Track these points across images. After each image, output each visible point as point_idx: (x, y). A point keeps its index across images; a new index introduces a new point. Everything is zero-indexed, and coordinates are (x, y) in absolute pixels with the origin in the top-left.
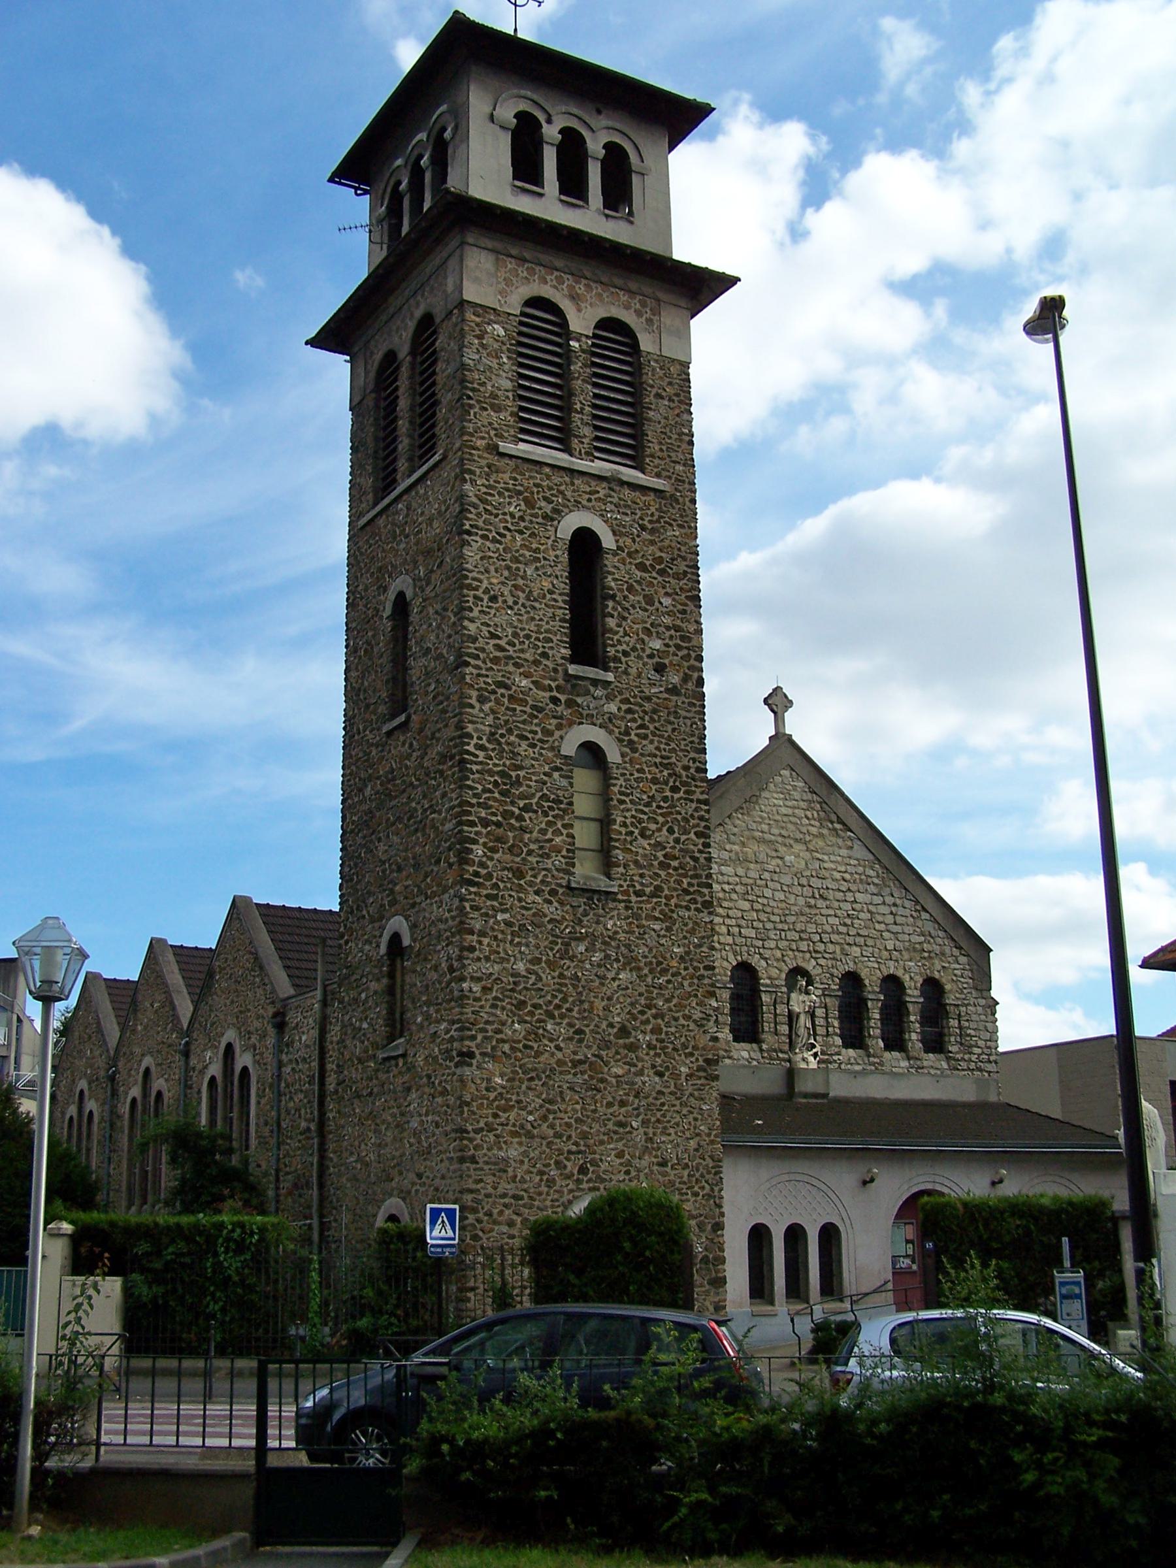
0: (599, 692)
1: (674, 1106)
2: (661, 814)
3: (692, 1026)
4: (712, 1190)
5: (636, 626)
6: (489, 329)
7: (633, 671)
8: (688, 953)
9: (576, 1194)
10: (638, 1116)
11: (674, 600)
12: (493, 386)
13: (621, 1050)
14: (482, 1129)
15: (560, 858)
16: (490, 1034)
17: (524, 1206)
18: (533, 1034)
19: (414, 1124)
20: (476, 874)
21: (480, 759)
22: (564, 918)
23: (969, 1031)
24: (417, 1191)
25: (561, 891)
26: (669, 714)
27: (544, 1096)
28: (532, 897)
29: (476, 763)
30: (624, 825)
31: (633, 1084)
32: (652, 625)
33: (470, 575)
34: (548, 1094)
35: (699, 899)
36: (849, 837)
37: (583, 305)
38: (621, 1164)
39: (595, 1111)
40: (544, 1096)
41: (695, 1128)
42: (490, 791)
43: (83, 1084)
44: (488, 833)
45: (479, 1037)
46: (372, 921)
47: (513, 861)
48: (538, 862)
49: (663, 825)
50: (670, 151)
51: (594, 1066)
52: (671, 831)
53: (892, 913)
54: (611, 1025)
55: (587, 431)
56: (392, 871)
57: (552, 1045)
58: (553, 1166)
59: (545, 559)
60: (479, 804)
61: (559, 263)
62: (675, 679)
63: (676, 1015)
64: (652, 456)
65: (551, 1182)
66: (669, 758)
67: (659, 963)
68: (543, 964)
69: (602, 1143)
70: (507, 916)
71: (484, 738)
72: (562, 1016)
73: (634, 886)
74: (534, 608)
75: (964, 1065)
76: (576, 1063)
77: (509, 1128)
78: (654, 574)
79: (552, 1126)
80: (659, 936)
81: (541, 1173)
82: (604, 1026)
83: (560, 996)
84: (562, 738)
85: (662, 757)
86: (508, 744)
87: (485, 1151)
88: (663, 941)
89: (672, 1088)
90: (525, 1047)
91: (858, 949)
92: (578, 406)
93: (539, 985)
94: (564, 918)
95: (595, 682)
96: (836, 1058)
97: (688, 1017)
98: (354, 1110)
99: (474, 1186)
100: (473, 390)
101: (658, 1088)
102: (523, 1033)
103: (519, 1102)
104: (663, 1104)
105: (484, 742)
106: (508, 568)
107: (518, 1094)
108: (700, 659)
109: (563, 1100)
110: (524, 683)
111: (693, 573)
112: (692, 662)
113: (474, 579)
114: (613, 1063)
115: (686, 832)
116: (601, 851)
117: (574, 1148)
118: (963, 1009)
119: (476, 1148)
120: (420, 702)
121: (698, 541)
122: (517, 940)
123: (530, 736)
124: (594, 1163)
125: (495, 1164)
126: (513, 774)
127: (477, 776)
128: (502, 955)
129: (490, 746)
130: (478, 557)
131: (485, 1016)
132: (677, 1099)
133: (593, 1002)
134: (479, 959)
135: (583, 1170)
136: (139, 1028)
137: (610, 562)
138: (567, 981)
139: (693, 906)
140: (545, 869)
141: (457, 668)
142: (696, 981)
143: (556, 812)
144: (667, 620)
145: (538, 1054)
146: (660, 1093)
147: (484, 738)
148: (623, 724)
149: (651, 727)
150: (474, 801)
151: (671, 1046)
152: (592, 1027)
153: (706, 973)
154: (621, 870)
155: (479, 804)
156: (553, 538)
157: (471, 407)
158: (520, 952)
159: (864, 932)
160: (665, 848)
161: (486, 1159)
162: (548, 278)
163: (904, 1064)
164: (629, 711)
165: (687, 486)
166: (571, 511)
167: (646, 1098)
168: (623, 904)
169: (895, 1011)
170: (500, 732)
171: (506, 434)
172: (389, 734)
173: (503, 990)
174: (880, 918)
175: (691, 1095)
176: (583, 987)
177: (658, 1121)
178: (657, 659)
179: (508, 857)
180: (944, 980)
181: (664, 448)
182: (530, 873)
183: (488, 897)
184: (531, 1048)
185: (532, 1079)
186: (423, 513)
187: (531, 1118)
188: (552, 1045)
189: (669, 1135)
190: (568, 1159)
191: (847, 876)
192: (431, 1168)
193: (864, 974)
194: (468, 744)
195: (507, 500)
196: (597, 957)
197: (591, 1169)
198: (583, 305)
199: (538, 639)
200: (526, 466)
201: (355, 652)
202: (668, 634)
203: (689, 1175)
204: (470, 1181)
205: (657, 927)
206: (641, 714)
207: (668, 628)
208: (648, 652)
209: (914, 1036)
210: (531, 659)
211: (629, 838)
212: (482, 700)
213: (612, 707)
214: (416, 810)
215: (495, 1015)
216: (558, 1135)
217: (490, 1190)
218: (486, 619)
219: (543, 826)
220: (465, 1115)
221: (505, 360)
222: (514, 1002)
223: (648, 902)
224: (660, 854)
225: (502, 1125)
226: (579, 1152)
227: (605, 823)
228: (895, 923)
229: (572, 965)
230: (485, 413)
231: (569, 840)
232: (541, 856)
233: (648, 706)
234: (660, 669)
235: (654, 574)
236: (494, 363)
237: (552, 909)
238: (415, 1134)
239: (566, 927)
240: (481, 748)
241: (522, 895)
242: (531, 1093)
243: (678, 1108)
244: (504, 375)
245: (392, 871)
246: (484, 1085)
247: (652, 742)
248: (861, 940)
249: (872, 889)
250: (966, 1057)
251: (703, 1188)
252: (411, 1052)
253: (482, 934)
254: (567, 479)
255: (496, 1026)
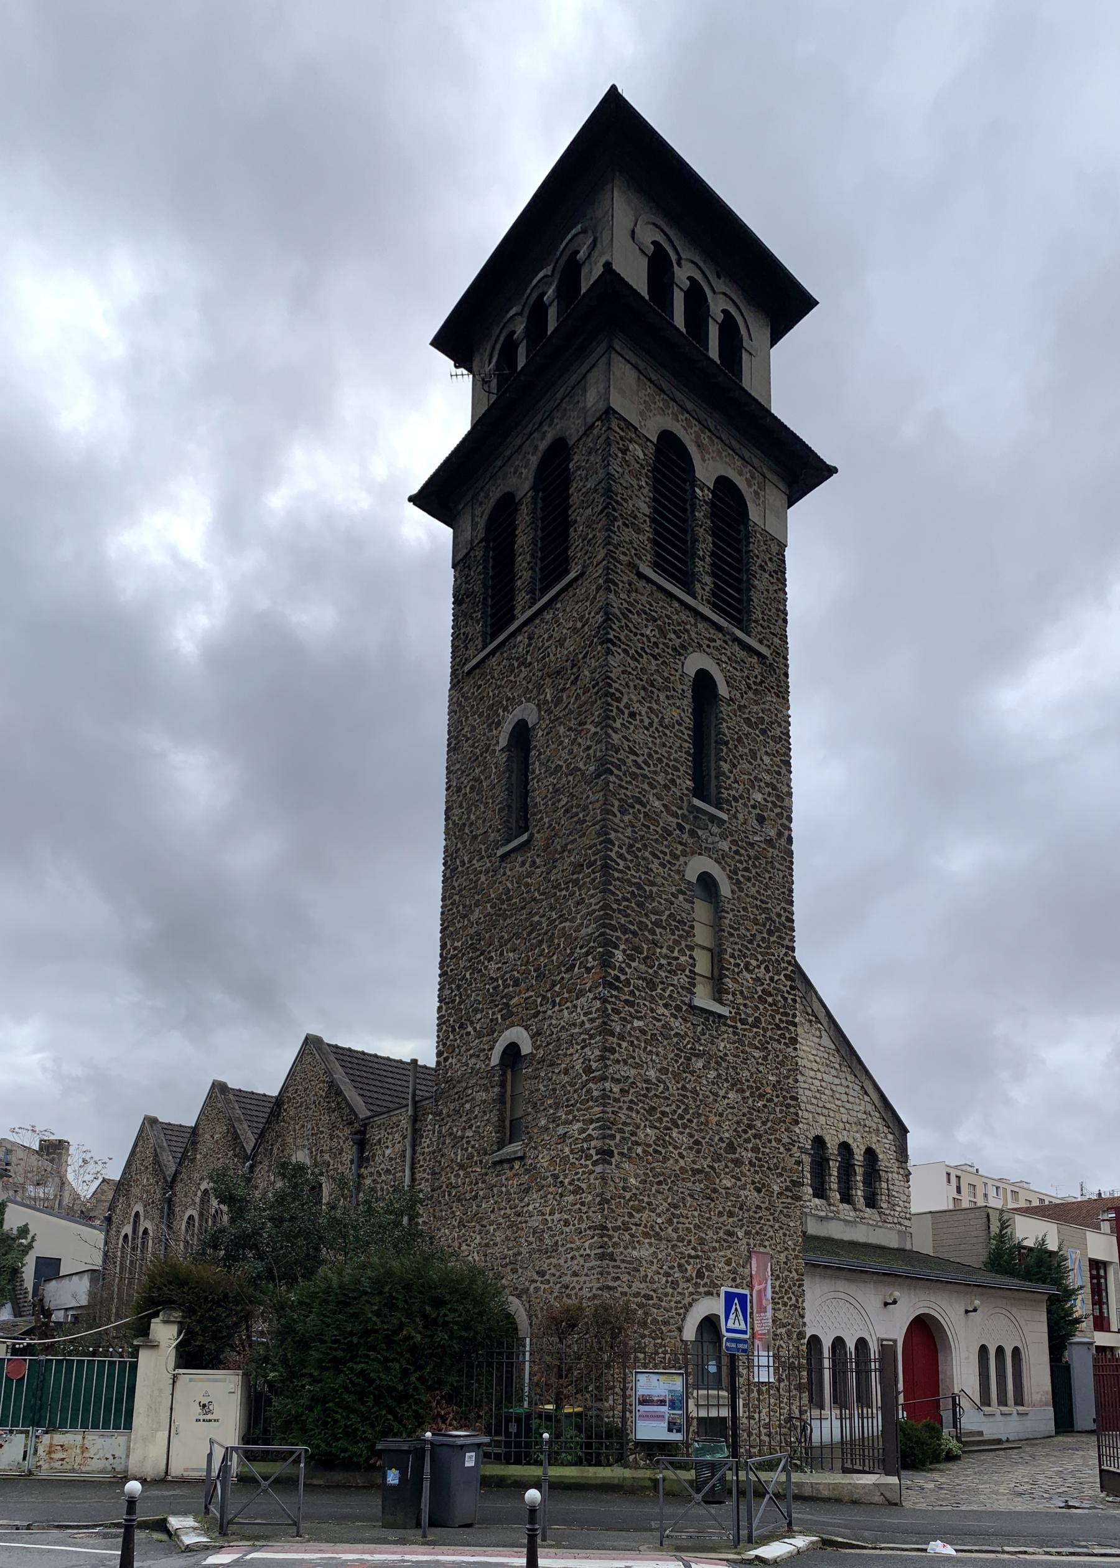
0: (715, 829)
1: (769, 1220)
2: (761, 953)
3: (782, 1149)
4: (797, 1301)
5: (743, 776)
6: (631, 447)
7: (740, 816)
8: (779, 1082)
9: (695, 1297)
10: (742, 1226)
11: (771, 760)
12: (634, 506)
13: (729, 1164)
14: (619, 1228)
15: (683, 976)
16: (627, 1135)
17: (654, 1306)
18: (661, 1141)
19: (535, 1222)
20: (617, 978)
21: (621, 867)
22: (686, 1034)
23: (894, 1193)
24: (537, 1289)
25: (685, 1008)
26: (767, 863)
27: (669, 1200)
28: (661, 1010)
29: (616, 870)
30: (733, 956)
31: (739, 1196)
32: (755, 777)
33: (614, 684)
34: (673, 1199)
35: (787, 1035)
36: (819, 1028)
37: (707, 456)
38: (729, 1271)
39: (709, 1219)
40: (669, 1200)
41: (784, 1242)
42: (627, 900)
43: (139, 1207)
44: (627, 940)
45: (618, 1137)
46: (479, 1035)
47: (647, 972)
48: (667, 977)
49: (762, 962)
50: (772, 346)
51: (707, 1175)
52: (767, 969)
53: (846, 1093)
54: (721, 1140)
55: (708, 579)
56: (506, 986)
57: (676, 1152)
58: (676, 1269)
59: (674, 690)
60: (620, 911)
61: (690, 406)
62: (773, 833)
63: (770, 1137)
64: (756, 622)
65: (675, 1284)
66: (767, 903)
67: (758, 1089)
68: (670, 1075)
69: (715, 1249)
70: (641, 1023)
71: (624, 848)
72: (685, 1126)
73: (740, 1015)
74: (665, 735)
75: (890, 1219)
76: (695, 1172)
77: (641, 1228)
78: (757, 732)
79: (676, 1230)
80: (758, 1063)
81: (667, 1275)
82: (716, 1139)
83: (683, 1107)
84: (686, 863)
85: (761, 901)
86: (644, 859)
87: (621, 1249)
88: (761, 1068)
89: (767, 1205)
90: (656, 1151)
91: (824, 1118)
92: (701, 553)
93: (666, 1094)
94: (686, 1034)
95: (713, 818)
96: (808, 1204)
97: (779, 1141)
98: (453, 1212)
99: (611, 1284)
100: (617, 502)
101: (757, 1203)
102: (654, 1138)
103: (649, 1204)
104: (761, 1218)
105: (624, 851)
106: (644, 689)
107: (649, 1196)
108: (790, 819)
109: (685, 1206)
110: (657, 803)
111: (785, 740)
112: (784, 821)
113: (617, 690)
114: (723, 1176)
115: (778, 974)
116: (712, 978)
117: (693, 1253)
118: (890, 1175)
119: (615, 1245)
120: (546, 820)
121: (790, 712)
122: (649, 1048)
123: (661, 856)
124: (709, 1268)
125: (630, 1263)
126: (648, 888)
127: (618, 883)
128: (637, 1060)
129: (629, 857)
130: (620, 669)
131: (623, 1117)
132: (771, 1214)
133: (708, 1117)
134: (618, 1061)
135: (700, 1275)
136: (198, 1157)
137: (724, 708)
138: (688, 1094)
139: (783, 1041)
140: (673, 985)
141: (598, 776)
142: (784, 1108)
143: (681, 932)
144: (767, 778)
145: (665, 1160)
146: (758, 1207)
147: (624, 848)
148: (733, 863)
149: (754, 872)
150: (615, 906)
151: (766, 1165)
152: (707, 1140)
153: (792, 1103)
154: (730, 997)
155: (620, 911)
156: (680, 672)
157: (616, 519)
158: (651, 1060)
159: (828, 1105)
160: (763, 984)
161: (622, 1257)
162: (680, 417)
163: (852, 1213)
164: (737, 852)
165: (781, 659)
166: (694, 651)
167: (748, 1211)
168: (731, 1029)
169: (847, 1170)
170: (637, 845)
171: (644, 558)
172: (504, 857)
173: (638, 1094)
174: (838, 1096)
175: (781, 1211)
176: (701, 1101)
177: (757, 1233)
178: (758, 811)
179: (643, 967)
180: (878, 1151)
181: (765, 618)
182: (661, 986)
183: (626, 1002)
184: (660, 1153)
185: (660, 1183)
186: (551, 637)
187: (659, 1221)
188: (676, 1152)
189: (765, 1247)
190: (689, 1263)
191: (818, 1059)
192: (557, 1267)
193: (827, 1139)
194: (611, 850)
195: (645, 622)
196: (712, 1074)
197: (706, 1274)
198: (707, 456)
199: (667, 765)
200: (660, 595)
201: (459, 790)
202: (767, 790)
203: (780, 1286)
204: (610, 1277)
205: (756, 1055)
206: (746, 858)
207: (767, 785)
208: (752, 802)
209: (859, 1193)
210: (662, 783)
211: (736, 970)
212: (623, 812)
213: (724, 845)
214: (539, 923)
215: (630, 1117)
216: (681, 1239)
217: (626, 1289)
218: (625, 732)
219: (670, 943)
220: (606, 1212)
221: (643, 484)
222: (647, 1107)
223: (751, 1031)
224: (759, 989)
225: (636, 1225)
226: (697, 1257)
227: (716, 955)
228: (848, 1101)
229: (693, 1079)
230: (627, 530)
231: (691, 961)
232: (669, 972)
233: (752, 853)
234: (761, 820)
235: (757, 732)
236: (635, 483)
237: (677, 1024)
238: (534, 1233)
239: (688, 1043)
240: (621, 856)
241: (653, 1006)
242: (660, 1197)
243: (771, 1223)
244: (643, 498)
245: (506, 986)
246: (621, 1184)
247: (754, 885)
248: (825, 1111)
249: (833, 1072)
250: (892, 1213)
251: (790, 1298)
252: (531, 1154)
253: (622, 1037)
254: (692, 621)
255: (631, 1128)
